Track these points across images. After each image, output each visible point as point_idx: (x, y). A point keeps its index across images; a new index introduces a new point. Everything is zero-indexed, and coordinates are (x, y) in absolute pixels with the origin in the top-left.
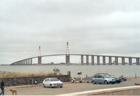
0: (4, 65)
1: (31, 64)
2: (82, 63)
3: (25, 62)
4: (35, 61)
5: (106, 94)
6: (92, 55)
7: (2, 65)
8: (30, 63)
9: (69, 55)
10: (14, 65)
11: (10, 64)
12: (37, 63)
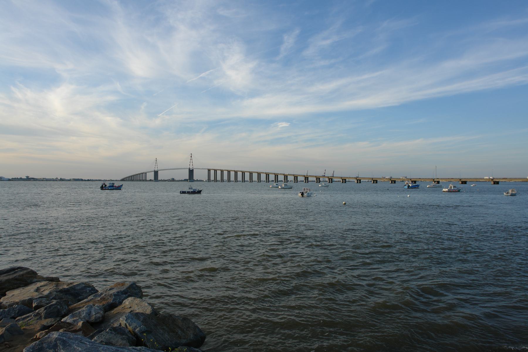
0: (34, 179)
1: (146, 180)
2: (209, 180)
3: (140, 177)
4: (151, 176)
5: (7, 180)
6: (250, 171)
7: (28, 179)
8: (144, 179)
9: (157, 172)
10: (125, 181)
11: (119, 179)
12: (153, 178)
